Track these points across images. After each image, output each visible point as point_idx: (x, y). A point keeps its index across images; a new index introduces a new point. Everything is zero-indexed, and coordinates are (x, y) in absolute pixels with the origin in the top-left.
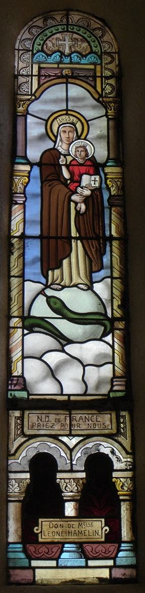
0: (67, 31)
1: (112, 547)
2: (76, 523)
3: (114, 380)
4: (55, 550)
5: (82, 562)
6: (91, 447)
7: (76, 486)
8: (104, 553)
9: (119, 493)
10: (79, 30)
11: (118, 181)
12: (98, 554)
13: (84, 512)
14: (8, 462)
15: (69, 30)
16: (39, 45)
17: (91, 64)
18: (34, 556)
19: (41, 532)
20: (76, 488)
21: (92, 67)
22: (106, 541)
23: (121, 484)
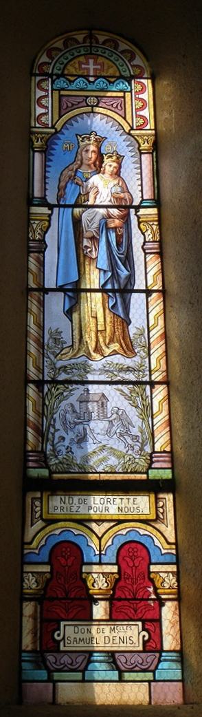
0: (91, 54)
1: (150, 657)
2: (107, 629)
3: (153, 455)
4: (80, 659)
5: (114, 675)
6: (142, 534)
7: (106, 582)
8: (141, 664)
9: (91, 591)
10: (105, 53)
11: (153, 224)
12: (62, 666)
13: (114, 617)
14: (22, 552)
15: (93, 52)
16: (59, 70)
17: (121, 91)
18: (53, 667)
19: (64, 638)
20: (106, 585)
21: (121, 94)
22: (144, 651)
23: (161, 581)
